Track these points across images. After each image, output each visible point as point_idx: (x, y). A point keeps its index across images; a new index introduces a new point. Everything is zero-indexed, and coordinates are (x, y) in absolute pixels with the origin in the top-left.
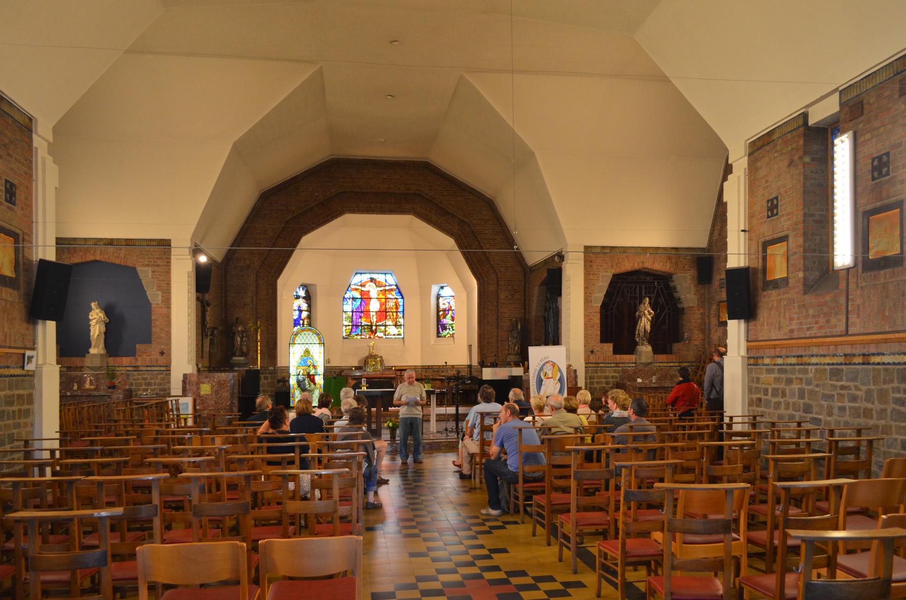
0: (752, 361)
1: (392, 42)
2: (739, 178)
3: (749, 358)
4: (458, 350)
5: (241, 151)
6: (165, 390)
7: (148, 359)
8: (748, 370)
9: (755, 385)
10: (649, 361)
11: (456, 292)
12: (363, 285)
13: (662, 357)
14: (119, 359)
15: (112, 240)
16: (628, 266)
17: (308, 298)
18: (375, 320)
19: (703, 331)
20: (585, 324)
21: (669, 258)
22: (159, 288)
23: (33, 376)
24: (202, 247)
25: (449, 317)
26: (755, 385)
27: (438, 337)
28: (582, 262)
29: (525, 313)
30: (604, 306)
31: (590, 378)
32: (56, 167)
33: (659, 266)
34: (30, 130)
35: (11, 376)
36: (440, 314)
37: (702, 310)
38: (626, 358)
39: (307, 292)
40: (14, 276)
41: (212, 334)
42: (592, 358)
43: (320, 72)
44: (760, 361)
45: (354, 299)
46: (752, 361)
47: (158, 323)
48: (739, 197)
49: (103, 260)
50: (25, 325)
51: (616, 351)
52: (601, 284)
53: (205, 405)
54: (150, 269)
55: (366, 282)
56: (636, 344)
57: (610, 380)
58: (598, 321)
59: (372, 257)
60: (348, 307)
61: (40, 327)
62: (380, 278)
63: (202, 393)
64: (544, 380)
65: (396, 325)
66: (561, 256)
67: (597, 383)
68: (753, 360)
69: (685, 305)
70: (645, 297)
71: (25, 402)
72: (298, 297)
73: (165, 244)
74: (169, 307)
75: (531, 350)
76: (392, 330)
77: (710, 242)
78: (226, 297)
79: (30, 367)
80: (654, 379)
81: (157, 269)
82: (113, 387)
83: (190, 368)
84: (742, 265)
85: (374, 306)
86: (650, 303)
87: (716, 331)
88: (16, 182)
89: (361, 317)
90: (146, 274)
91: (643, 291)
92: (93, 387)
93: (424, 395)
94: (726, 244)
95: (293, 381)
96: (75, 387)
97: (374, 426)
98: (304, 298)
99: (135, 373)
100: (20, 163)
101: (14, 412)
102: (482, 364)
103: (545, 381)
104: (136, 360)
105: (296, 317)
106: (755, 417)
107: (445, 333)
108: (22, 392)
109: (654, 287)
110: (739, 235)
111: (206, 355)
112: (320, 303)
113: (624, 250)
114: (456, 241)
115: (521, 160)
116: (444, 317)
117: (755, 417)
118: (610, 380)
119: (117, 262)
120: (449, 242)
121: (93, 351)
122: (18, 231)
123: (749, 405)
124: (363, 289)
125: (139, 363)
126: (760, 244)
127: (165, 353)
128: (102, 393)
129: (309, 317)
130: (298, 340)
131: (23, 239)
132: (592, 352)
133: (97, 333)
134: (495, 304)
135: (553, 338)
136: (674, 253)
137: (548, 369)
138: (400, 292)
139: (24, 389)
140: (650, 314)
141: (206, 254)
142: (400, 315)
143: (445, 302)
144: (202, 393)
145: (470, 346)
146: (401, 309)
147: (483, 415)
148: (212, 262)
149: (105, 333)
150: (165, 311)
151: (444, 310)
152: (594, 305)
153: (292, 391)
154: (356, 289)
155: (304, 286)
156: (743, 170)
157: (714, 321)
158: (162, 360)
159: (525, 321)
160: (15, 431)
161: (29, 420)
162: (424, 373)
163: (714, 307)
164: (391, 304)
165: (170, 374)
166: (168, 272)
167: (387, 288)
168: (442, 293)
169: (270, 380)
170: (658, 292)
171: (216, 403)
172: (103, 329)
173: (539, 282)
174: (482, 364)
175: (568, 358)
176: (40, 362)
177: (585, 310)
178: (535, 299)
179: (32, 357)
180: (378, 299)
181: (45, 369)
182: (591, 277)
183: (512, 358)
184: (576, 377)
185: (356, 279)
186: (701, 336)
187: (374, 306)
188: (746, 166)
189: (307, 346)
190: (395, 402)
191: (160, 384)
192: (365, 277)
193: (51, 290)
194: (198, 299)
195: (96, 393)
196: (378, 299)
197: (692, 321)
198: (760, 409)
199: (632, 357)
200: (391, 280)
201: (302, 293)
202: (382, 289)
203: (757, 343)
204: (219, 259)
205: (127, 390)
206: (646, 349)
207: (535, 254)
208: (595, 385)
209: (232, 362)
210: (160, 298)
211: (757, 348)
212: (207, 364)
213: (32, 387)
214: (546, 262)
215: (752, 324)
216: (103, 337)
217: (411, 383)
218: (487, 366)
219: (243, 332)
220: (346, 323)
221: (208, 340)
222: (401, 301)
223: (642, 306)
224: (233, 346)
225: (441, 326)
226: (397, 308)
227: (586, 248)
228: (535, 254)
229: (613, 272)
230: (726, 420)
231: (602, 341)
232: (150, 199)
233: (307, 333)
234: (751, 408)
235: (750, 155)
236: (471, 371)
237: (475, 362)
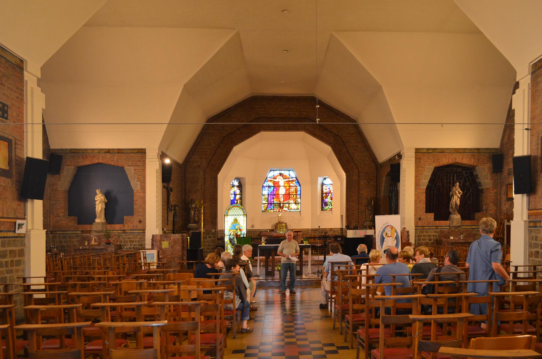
0: (532, 224)
1: (283, 11)
2: (524, 90)
3: (530, 222)
4: (334, 219)
5: (191, 91)
6: (141, 245)
7: (131, 225)
8: (529, 230)
9: (534, 242)
10: (459, 225)
11: (333, 181)
12: (275, 178)
13: (468, 222)
14: (113, 226)
15: (109, 149)
16: (445, 161)
17: (240, 186)
18: (282, 200)
19: (496, 205)
20: (415, 201)
21: (473, 156)
22: (139, 180)
23: (24, 237)
24: (167, 153)
25: (329, 197)
26: (534, 242)
27: (322, 210)
28: (414, 159)
29: (377, 194)
30: (428, 188)
31: (418, 236)
32: (43, 95)
33: (466, 161)
34: (22, 69)
35: (4, 237)
36: (324, 196)
37: (495, 191)
38: (443, 223)
39: (240, 183)
40: (8, 168)
41: (174, 210)
42: (420, 224)
43: (238, 34)
44: (538, 224)
45: (269, 187)
46: (532, 224)
47: (137, 202)
48: (524, 105)
49: (104, 163)
50: (17, 203)
51: (436, 219)
52: (426, 173)
53: (165, 255)
54: (133, 168)
55: (277, 176)
56: (450, 213)
57: (432, 237)
58: (424, 199)
59: (281, 161)
60: (266, 192)
61: (29, 204)
62: (286, 173)
63: (163, 247)
64: (386, 238)
65: (295, 203)
66: (400, 156)
67: (423, 240)
68: (533, 224)
69: (484, 187)
70: (456, 182)
71: (21, 254)
72: (233, 186)
73: (142, 152)
74: (145, 192)
75: (377, 218)
76: (293, 206)
77: (502, 144)
78: (185, 185)
79: (22, 231)
80: (462, 237)
81: (137, 168)
82: (109, 243)
83: (158, 231)
84: (525, 154)
85: (282, 191)
86: (460, 186)
87: (505, 204)
88: (8, 103)
89: (273, 198)
90: (130, 171)
91: (455, 178)
92: (96, 243)
93: (298, 249)
94: (513, 140)
95: (227, 239)
96: (86, 244)
97: (270, 269)
98: (238, 186)
99: (123, 234)
100: (12, 90)
101: (6, 262)
102: (348, 227)
103: (386, 239)
104: (124, 226)
105: (232, 199)
106: (535, 267)
107: (326, 208)
108: (13, 248)
109: (463, 175)
110: (523, 133)
111: (171, 223)
112: (248, 189)
113: (442, 151)
114: (332, 147)
115: (373, 92)
116: (326, 198)
117: (535, 267)
118: (432, 237)
119: (113, 164)
120: (328, 149)
121: (97, 220)
122: (10, 138)
123: (530, 256)
124: (275, 180)
125: (126, 228)
126: (540, 138)
127: (142, 222)
128: (101, 247)
129: (241, 198)
130: (230, 213)
131: (15, 144)
132: (420, 219)
133: (100, 209)
134: (357, 188)
135: (394, 209)
136: (476, 152)
137: (388, 230)
138: (298, 182)
139: (16, 246)
140: (460, 193)
141: (170, 158)
142: (298, 196)
143: (327, 188)
144: (163, 247)
145: (342, 216)
146: (299, 193)
147: (333, 264)
148: (174, 162)
149: (105, 209)
150: (142, 195)
151: (326, 193)
152: (421, 187)
153: (226, 245)
154: (271, 181)
155: (237, 179)
156: (527, 85)
157: (504, 198)
158: (140, 226)
159: (377, 200)
160: (8, 275)
161: (20, 267)
162: (313, 234)
163: (504, 188)
164: (293, 190)
165: (145, 235)
166: (144, 170)
167: (290, 179)
168: (325, 182)
169: (212, 239)
170: (465, 178)
171: (172, 253)
172: (104, 206)
173: (386, 174)
174: (348, 227)
175: (403, 222)
176: (30, 227)
177: (415, 191)
178: (383, 184)
179: (23, 224)
180: (283, 185)
181: (32, 232)
182: (420, 169)
183: (367, 224)
184: (408, 236)
185: (271, 174)
186: (494, 208)
187: (282, 191)
188: (529, 82)
189: (236, 217)
190: (278, 253)
191: (139, 241)
192: (277, 173)
193: (32, 179)
194: (164, 187)
195: (97, 247)
196: (283, 185)
197: (489, 198)
198: (537, 259)
199: (447, 222)
200: (293, 174)
201: (236, 183)
202: (287, 180)
203: (536, 211)
204: (181, 161)
205: (118, 245)
206: (456, 217)
207: (383, 154)
208: (422, 241)
209: (188, 227)
210: (139, 186)
211: (536, 215)
212: (170, 227)
213: (24, 245)
214: (390, 160)
215: (532, 197)
216: (104, 211)
217: (290, 241)
218: (351, 229)
219: (195, 208)
220: (264, 202)
221: (172, 213)
222: (299, 188)
223: (454, 188)
224: (189, 216)
225: (324, 204)
226: (296, 192)
227: (416, 149)
228: (383, 154)
229: (435, 165)
230: (512, 269)
231: (427, 212)
232: (135, 124)
233: (236, 208)
234: (531, 259)
235: (532, 73)
236: (342, 232)
237: (344, 227)
